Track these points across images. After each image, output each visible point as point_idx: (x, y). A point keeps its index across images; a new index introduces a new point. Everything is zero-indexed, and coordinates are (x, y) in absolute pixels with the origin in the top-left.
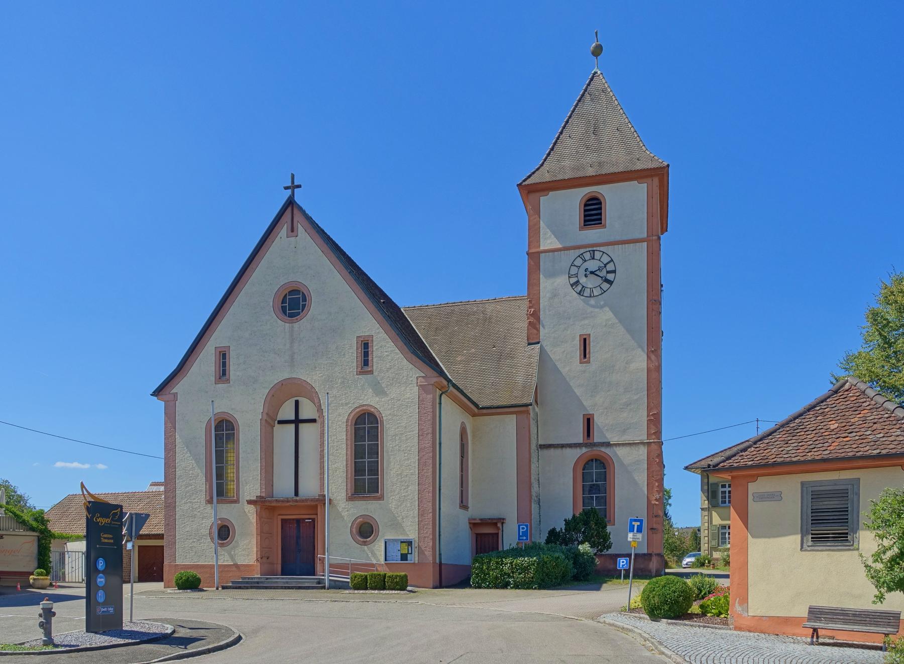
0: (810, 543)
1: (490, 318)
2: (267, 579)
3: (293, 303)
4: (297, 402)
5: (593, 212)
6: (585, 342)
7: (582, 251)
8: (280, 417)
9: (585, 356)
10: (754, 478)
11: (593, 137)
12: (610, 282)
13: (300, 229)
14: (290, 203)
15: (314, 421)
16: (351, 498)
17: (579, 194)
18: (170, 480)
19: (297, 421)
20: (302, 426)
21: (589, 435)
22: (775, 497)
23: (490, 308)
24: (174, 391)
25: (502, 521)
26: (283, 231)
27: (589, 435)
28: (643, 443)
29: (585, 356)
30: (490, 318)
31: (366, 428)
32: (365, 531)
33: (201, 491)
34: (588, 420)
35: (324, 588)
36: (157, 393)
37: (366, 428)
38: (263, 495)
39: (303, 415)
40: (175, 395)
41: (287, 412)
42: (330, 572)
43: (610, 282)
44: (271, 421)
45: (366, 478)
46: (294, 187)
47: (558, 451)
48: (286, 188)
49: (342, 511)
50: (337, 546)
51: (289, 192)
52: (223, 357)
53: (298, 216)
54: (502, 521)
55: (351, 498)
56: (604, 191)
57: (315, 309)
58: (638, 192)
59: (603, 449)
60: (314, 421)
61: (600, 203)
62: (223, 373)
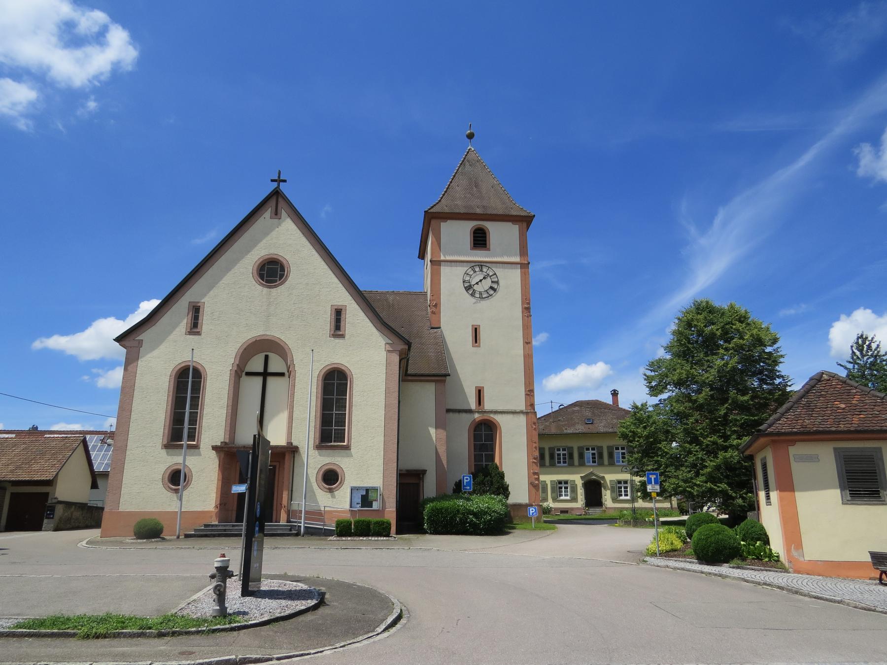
0: (849, 498)
1: (393, 305)
2: (233, 526)
3: (272, 272)
4: (267, 357)
5: (480, 240)
6: (476, 331)
7: (473, 264)
8: (249, 369)
9: (476, 342)
10: (793, 443)
11: (475, 189)
12: (495, 290)
13: (284, 214)
14: (276, 194)
15: (282, 375)
16: (318, 447)
17: (469, 225)
18: (485, 412)
19: (265, 374)
20: (271, 381)
21: (480, 404)
22: (814, 459)
23: (391, 298)
24: (140, 338)
25: (424, 472)
26: (267, 214)
27: (480, 404)
28: (522, 412)
29: (476, 342)
30: (393, 305)
31: (335, 384)
32: (331, 478)
33: (157, 435)
34: (480, 391)
35: (298, 535)
36: (120, 339)
37: (335, 384)
38: (227, 441)
39: (271, 369)
40: (140, 342)
41: (256, 364)
42: (306, 519)
43: (495, 290)
44: (240, 372)
45: (332, 429)
46: (279, 181)
47: (456, 415)
48: (272, 181)
49: (312, 461)
50: (309, 496)
51: (275, 185)
52: (196, 311)
53: (281, 203)
54: (424, 472)
55: (318, 447)
56: (490, 226)
57: (294, 278)
58: (512, 231)
59: (492, 415)
60: (282, 375)
61: (485, 233)
62: (195, 327)
